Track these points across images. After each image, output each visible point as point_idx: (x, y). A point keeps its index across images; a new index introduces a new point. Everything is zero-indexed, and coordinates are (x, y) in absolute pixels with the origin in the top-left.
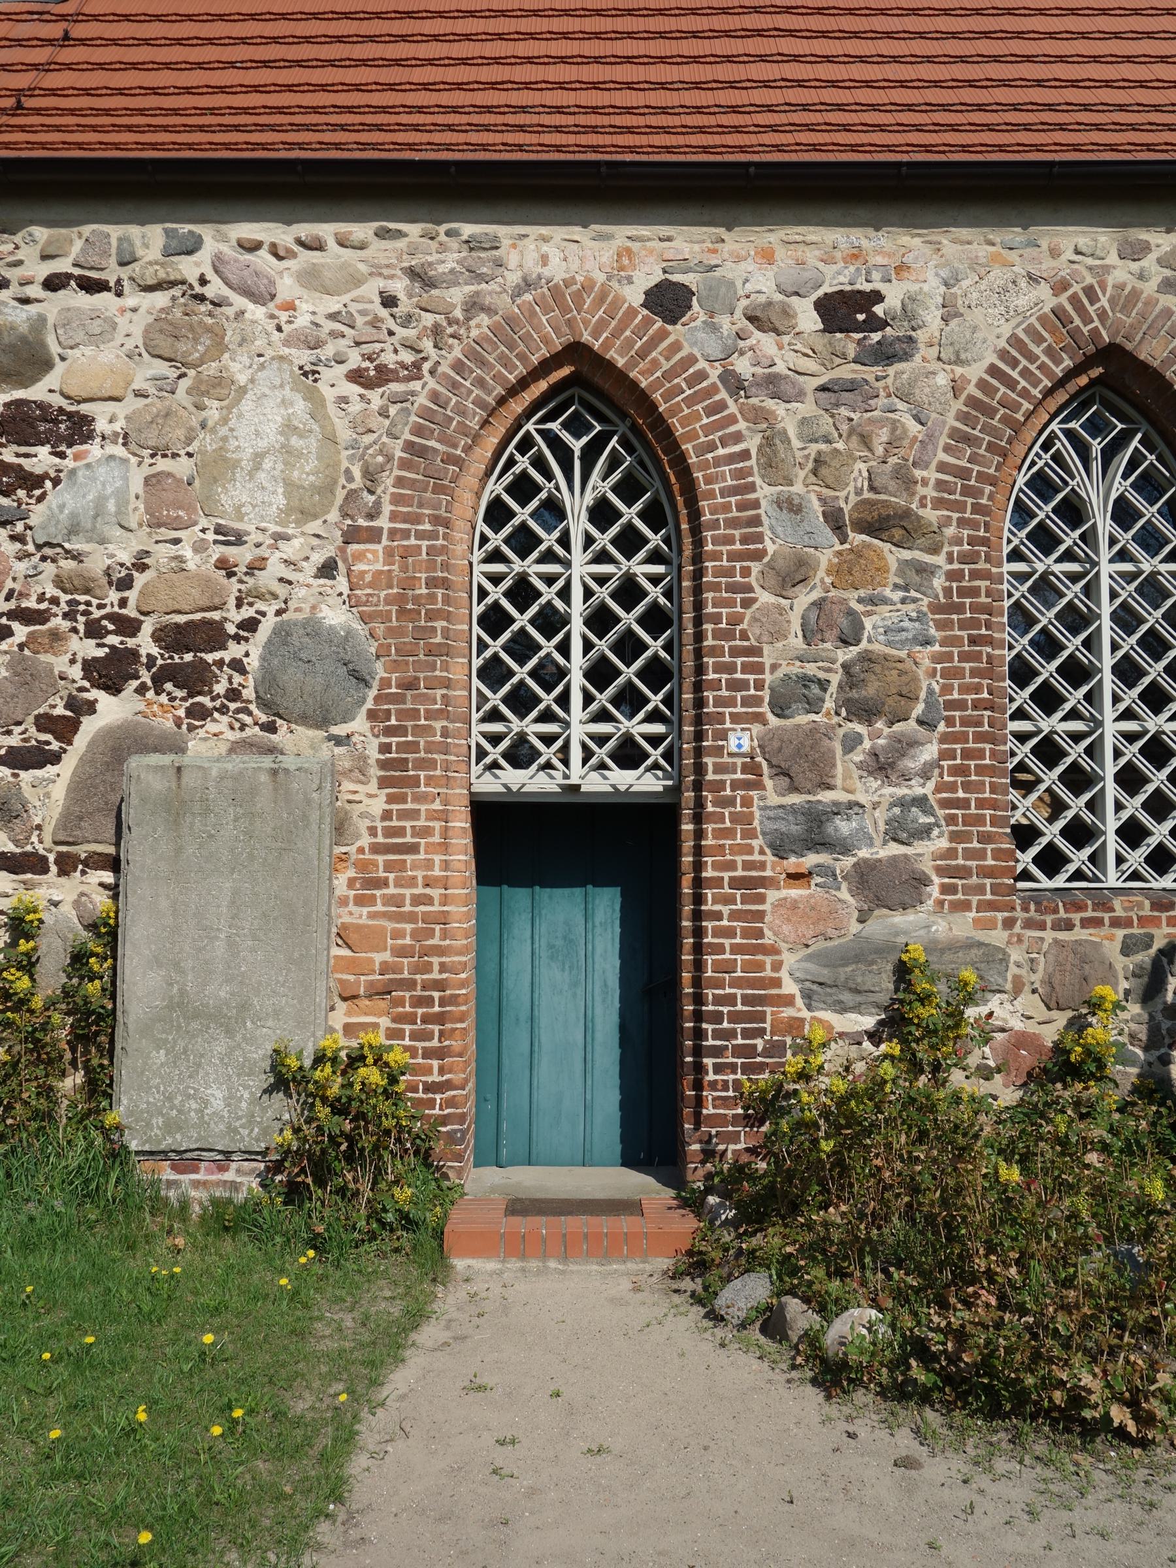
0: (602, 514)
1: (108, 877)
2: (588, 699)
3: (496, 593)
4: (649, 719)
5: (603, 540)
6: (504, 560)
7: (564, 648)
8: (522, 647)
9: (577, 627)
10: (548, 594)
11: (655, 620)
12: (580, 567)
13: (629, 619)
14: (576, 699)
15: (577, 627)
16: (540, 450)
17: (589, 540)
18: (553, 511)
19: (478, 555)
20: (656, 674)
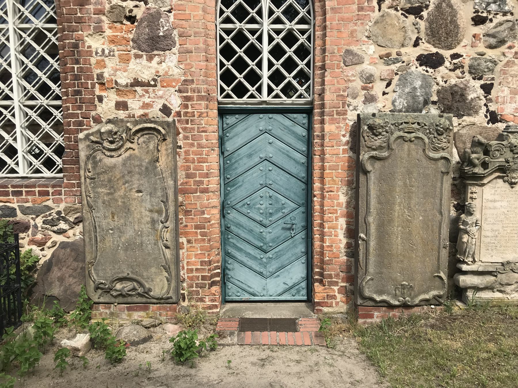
1: (461, 70)
6: (282, 22)
7: (259, 65)
9: (266, 55)
10: (252, 39)
12: (266, 26)
15: (266, 55)
17: (271, 12)
19: (219, 20)
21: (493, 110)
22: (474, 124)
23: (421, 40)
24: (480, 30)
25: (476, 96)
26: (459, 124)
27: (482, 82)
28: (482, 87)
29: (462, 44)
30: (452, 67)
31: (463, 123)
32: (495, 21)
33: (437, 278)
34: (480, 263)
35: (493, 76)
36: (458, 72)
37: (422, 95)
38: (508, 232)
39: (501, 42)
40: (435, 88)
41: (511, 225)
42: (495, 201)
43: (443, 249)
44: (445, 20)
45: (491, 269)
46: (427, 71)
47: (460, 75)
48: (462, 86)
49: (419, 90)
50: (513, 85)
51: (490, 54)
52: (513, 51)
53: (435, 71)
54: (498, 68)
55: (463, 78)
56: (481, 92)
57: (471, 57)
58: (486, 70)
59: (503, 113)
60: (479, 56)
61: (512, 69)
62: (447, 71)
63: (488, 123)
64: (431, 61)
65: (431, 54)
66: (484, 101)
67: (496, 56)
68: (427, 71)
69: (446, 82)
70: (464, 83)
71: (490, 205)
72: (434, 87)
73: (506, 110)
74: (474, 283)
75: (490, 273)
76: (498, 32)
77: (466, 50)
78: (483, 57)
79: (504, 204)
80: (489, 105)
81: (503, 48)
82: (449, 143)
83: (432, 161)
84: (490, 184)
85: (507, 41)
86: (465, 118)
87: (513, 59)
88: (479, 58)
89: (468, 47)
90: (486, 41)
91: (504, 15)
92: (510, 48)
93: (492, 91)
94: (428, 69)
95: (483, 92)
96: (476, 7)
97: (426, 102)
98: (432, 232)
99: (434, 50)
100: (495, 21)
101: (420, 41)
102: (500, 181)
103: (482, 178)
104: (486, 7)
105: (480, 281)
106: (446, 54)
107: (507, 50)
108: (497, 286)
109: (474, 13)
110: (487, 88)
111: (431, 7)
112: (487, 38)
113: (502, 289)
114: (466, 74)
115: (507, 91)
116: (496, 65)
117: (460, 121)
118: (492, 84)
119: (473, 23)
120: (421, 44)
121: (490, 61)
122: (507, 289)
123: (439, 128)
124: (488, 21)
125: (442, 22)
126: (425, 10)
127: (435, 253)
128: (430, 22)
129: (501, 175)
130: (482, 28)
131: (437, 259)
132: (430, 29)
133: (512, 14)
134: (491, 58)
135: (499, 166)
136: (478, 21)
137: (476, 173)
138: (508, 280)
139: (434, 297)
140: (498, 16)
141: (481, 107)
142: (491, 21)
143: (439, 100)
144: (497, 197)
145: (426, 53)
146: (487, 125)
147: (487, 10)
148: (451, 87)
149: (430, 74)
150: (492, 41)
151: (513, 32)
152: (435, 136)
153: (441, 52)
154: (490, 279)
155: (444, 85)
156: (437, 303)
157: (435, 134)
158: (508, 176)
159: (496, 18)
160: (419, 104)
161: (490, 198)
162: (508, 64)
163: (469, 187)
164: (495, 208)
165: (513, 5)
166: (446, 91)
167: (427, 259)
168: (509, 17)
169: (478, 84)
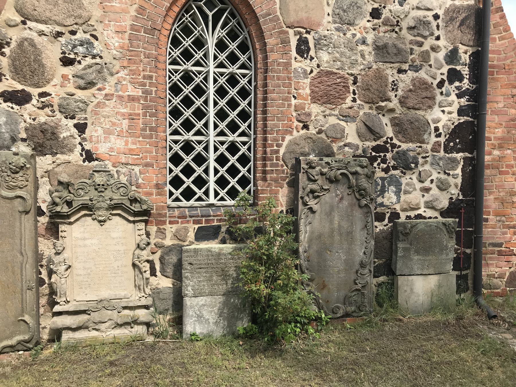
0: (221, 46)
1: (50, 108)
2: (216, 126)
3: (177, 148)
4: (241, 135)
5: (222, 126)
7: (206, 171)
8: (188, 171)
11: (244, 160)
12: (212, 67)
13: (233, 160)
14: (211, 126)
16: (195, 12)
18: (199, 43)
19: (169, 131)
20: (244, 116)
21: (89, 149)
22: (70, 162)
23: (5, 76)
24: (68, 71)
25: (69, 134)
26: (54, 162)
27: (75, 121)
28: (76, 126)
29: (52, 83)
30: (40, 105)
31: (57, 161)
32: (84, 63)
33: (22, 322)
34: (75, 303)
35: (86, 116)
36: (47, 110)
37: (8, 132)
38: (101, 269)
39: (89, 83)
40: (23, 125)
41: (104, 262)
42: (85, 239)
43: (28, 291)
44: (28, 58)
45: (83, 308)
46: (12, 108)
47: (50, 113)
48: (52, 124)
49: (4, 126)
50: (106, 125)
51: (80, 95)
52: (104, 92)
53: (21, 108)
54: (89, 109)
55: (53, 117)
56: (75, 131)
57: (61, 96)
58: (77, 110)
59: (98, 152)
60: (68, 96)
61: (104, 110)
62: (35, 109)
63: (84, 161)
64: (20, 98)
65: (16, 91)
66: (79, 140)
67: (85, 96)
68: (12, 108)
69: (34, 120)
70: (55, 121)
71: (81, 243)
72: (22, 124)
73: (100, 149)
74: (65, 323)
75: (84, 312)
76: (85, 74)
77: (56, 90)
78: (73, 97)
79: (95, 241)
80: (83, 144)
81: (93, 90)
82: (27, 181)
83: (7, 200)
84: (78, 222)
85: (97, 83)
86: (58, 156)
87: (104, 101)
88: (69, 98)
89: (58, 87)
90: (76, 82)
91: (92, 58)
92: (99, 89)
93: (87, 131)
94: (14, 106)
95: (77, 131)
96: (63, 48)
97: (14, 140)
98: (13, 273)
99: (20, 87)
100: (84, 63)
101: (3, 77)
102: (89, 219)
103: (68, 217)
104: (73, 49)
105: (72, 321)
106: (35, 92)
107: (97, 92)
108: (91, 325)
109: (62, 54)
110: (81, 128)
111: (13, 45)
112: (77, 79)
113: (97, 327)
114: (56, 113)
115: (100, 131)
116: (87, 105)
117: (54, 159)
118: (86, 124)
119: (61, 63)
120: (4, 80)
121: (81, 101)
122: (101, 327)
123: (11, 166)
124: (76, 63)
125: (24, 60)
126: (6, 46)
127: (18, 295)
128: (13, 60)
129: (88, 213)
130: (72, 69)
131: (20, 302)
132: (13, 65)
133: (101, 57)
134: (80, 99)
135: (81, 204)
136: (67, 62)
137: (59, 212)
138: (100, 318)
139: (19, 343)
140: (86, 59)
141: (75, 145)
142: (79, 62)
143: (28, 137)
144: (87, 235)
145: (10, 90)
146: (82, 163)
147: (73, 52)
148: (41, 125)
149: (15, 110)
150: (82, 82)
151: (102, 74)
152: (9, 174)
153: (28, 89)
154: (83, 318)
155: (33, 123)
156: (25, 348)
157: (9, 172)
158: (94, 214)
159: (85, 60)
160: (5, 140)
161: (79, 236)
162: (98, 105)
163: (60, 226)
164: (85, 246)
165: (101, 49)
166: (35, 128)
167: (9, 302)
168: (98, 60)
169: (71, 123)
